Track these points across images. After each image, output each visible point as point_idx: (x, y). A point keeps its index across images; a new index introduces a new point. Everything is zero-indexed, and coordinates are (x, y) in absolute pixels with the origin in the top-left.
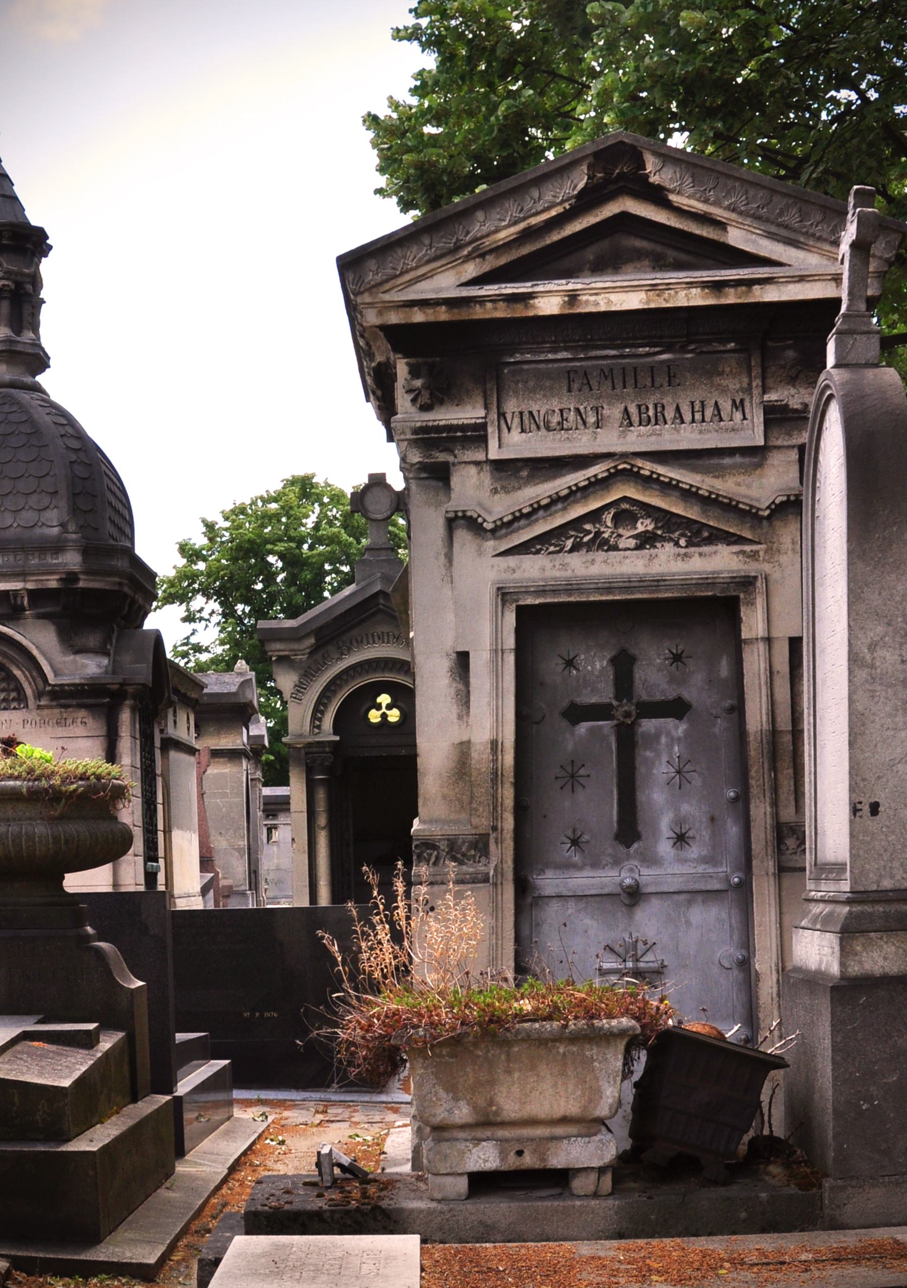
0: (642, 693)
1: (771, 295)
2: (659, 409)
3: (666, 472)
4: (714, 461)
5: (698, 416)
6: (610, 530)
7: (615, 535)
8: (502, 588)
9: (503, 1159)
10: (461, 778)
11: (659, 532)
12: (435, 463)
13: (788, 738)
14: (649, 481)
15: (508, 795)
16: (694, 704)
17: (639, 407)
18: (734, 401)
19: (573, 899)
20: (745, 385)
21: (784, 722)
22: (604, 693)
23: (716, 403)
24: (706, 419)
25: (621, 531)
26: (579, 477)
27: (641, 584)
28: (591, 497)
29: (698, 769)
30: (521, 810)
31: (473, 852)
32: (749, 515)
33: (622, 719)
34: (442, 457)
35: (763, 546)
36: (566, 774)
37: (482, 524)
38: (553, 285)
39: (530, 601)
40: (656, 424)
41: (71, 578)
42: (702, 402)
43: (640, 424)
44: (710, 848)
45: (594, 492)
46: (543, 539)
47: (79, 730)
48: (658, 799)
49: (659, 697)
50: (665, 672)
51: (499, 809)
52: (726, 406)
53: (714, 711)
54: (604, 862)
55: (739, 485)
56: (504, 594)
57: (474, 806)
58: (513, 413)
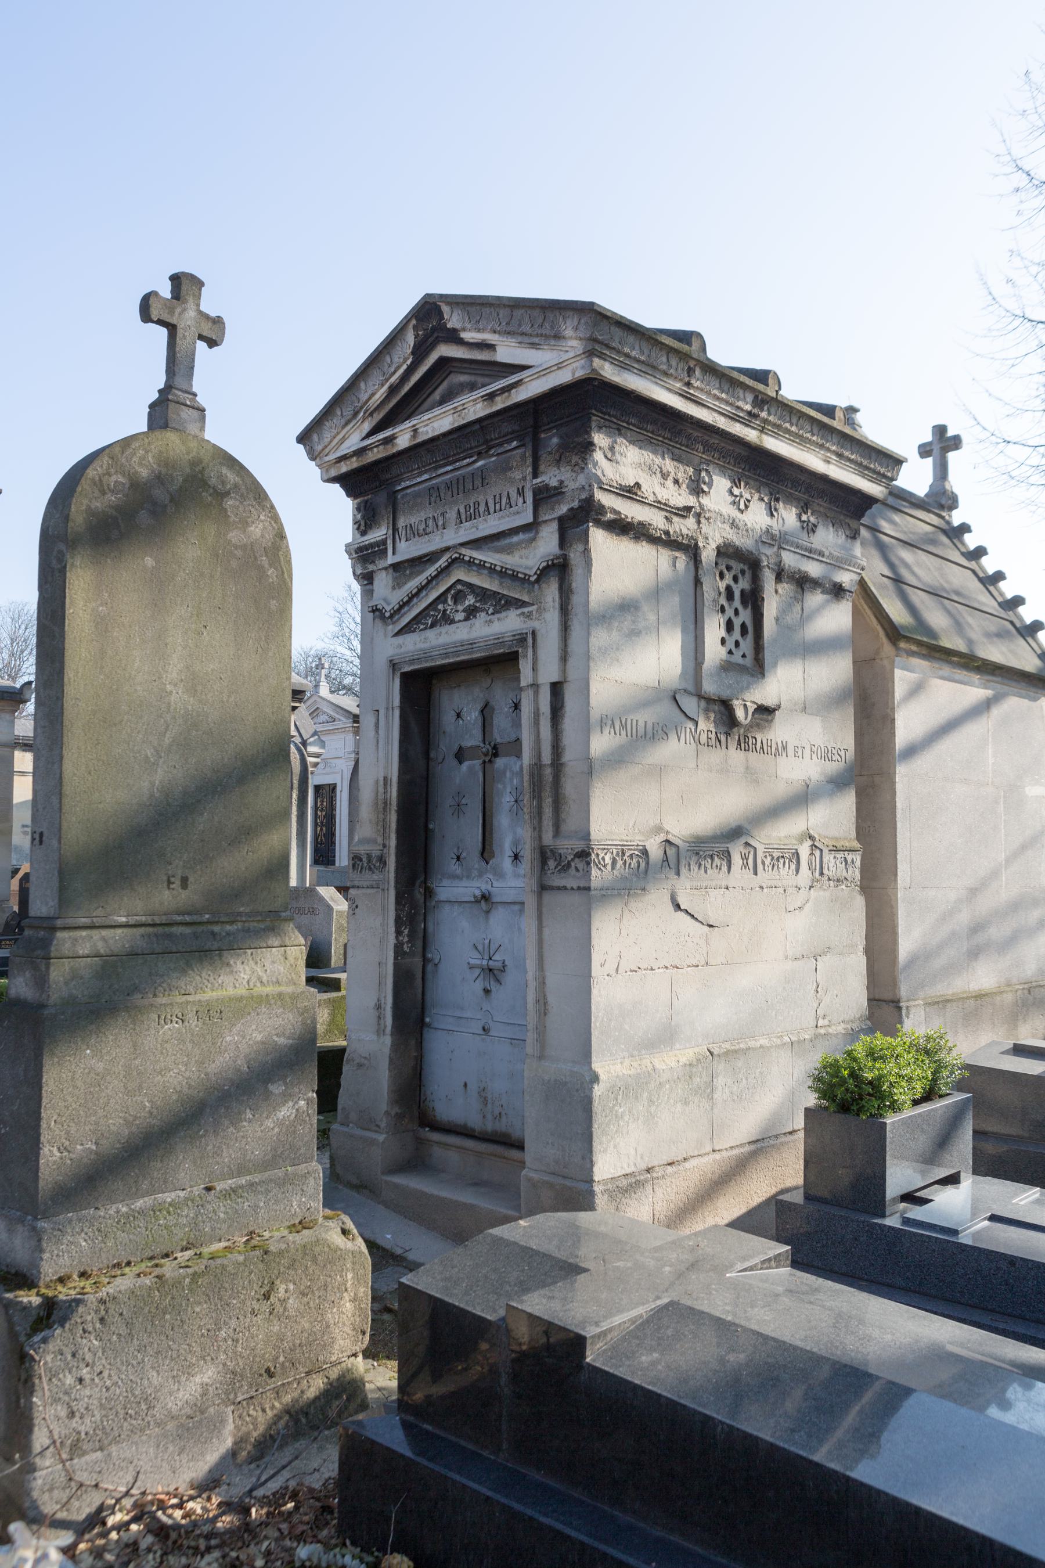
1: (521, 395)
3: (478, 555)
4: (507, 541)
9: (605, 1182)
13: (548, 772)
26: (432, 570)
35: (535, 607)
38: (402, 427)
39: (407, 668)
46: (416, 619)
52: (514, 494)
56: (394, 665)
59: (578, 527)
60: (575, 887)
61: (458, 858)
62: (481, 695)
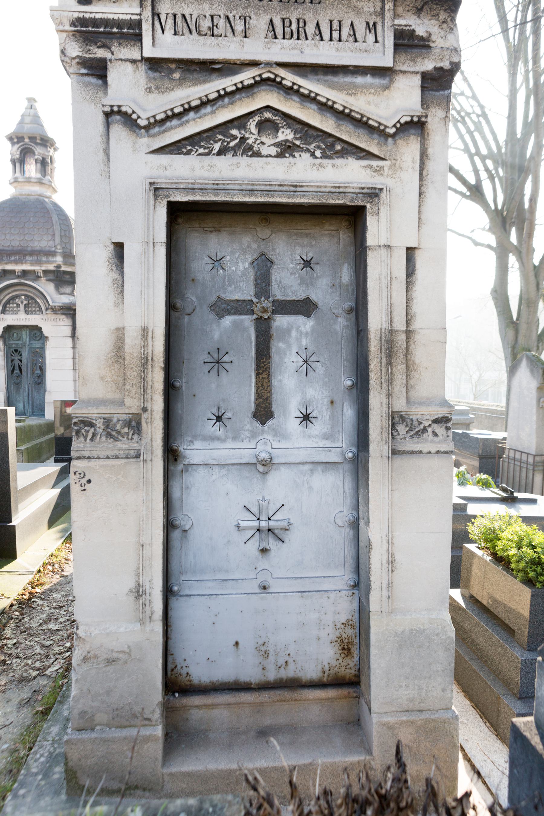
0: (277, 293)
2: (301, 24)
3: (308, 85)
4: (349, 79)
5: (336, 35)
6: (254, 137)
7: (258, 142)
8: (154, 183)
10: (116, 362)
11: (298, 143)
12: (94, 59)
13: (402, 337)
14: (291, 91)
15: (157, 378)
16: (320, 304)
17: (283, 20)
18: (368, 23)
19: (217, 466)
20: (378, 9)
21: (400, 324)
22: (245, 291)
23: (352, 24)
24: (342, 38)
25: (263, 139)
26: (228, 83)
27: (281, 188)
28: (238, 103)
29: (322, 360)
30: (170, 390)
31: (126, 430)
32: (376, 131)
33: (260, 314)
34: (101, 53)
36: (213, 360)
37: (136, 120)
40: (298, 39)
41: (59, 266)
42: (340, 22)
43: (284, 38)
44: (330, 427)
45: (241, 99)
46: (193, 140)
47: (62, 323)
48: (291, 386)
49: (291, 297)
50: (297, 276)
51: (149, 391)
52: (360, 28)
53: (336, 311)
54: (243, 436)
55: (369, 103)
56: (156, 189)
57: (127, 387)
58: (167, 14)
59: (437, 91)
60: (433, 451)
61: (219, 419)
62: (254, 246)
